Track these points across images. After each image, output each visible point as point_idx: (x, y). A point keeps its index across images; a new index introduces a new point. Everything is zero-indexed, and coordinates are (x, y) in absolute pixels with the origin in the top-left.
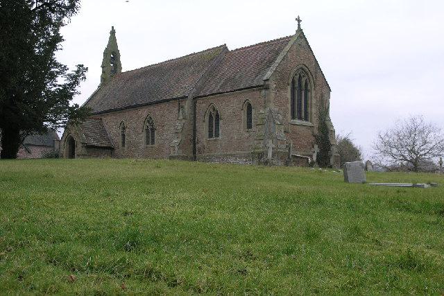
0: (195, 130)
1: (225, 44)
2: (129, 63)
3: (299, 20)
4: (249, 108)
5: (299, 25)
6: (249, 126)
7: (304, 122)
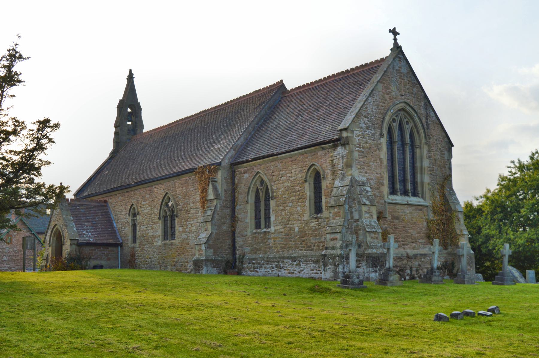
0: (233, 218)
1: (282, 81)
2: (151, 121)
3: (394, 32)
4: (318, 178)
5: (395, 39)
6: (318, 208)
7: (413, 200)
